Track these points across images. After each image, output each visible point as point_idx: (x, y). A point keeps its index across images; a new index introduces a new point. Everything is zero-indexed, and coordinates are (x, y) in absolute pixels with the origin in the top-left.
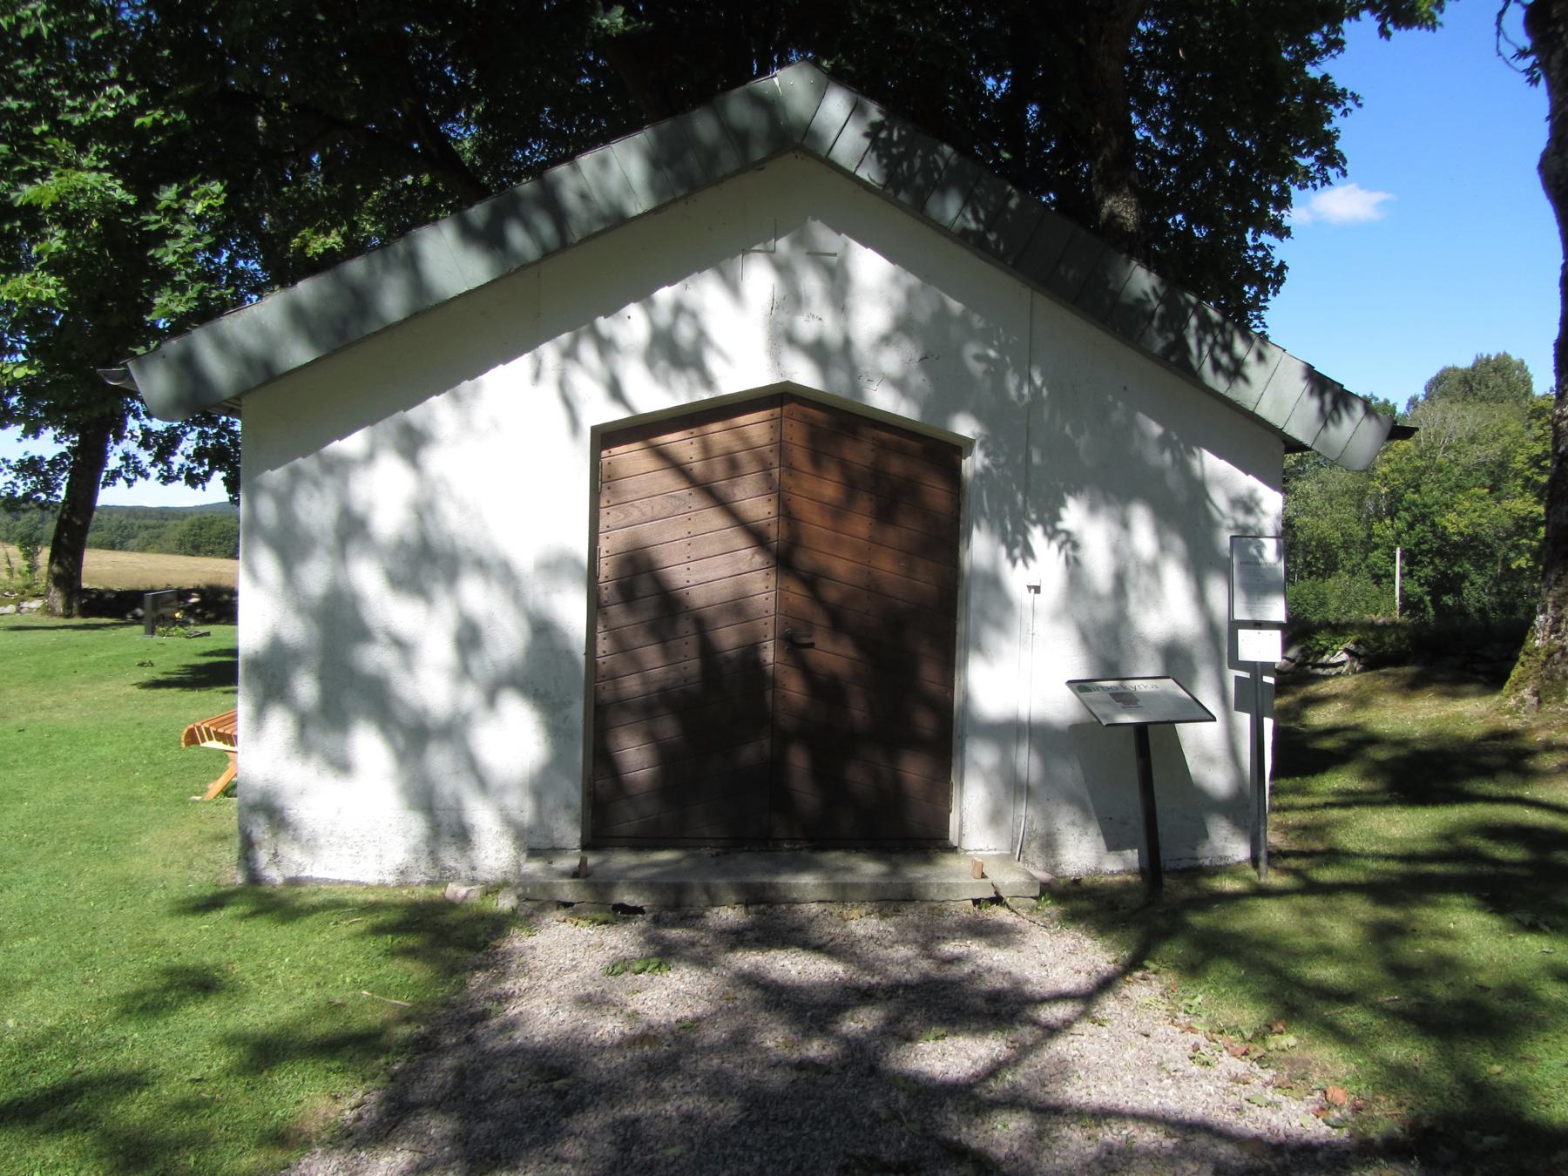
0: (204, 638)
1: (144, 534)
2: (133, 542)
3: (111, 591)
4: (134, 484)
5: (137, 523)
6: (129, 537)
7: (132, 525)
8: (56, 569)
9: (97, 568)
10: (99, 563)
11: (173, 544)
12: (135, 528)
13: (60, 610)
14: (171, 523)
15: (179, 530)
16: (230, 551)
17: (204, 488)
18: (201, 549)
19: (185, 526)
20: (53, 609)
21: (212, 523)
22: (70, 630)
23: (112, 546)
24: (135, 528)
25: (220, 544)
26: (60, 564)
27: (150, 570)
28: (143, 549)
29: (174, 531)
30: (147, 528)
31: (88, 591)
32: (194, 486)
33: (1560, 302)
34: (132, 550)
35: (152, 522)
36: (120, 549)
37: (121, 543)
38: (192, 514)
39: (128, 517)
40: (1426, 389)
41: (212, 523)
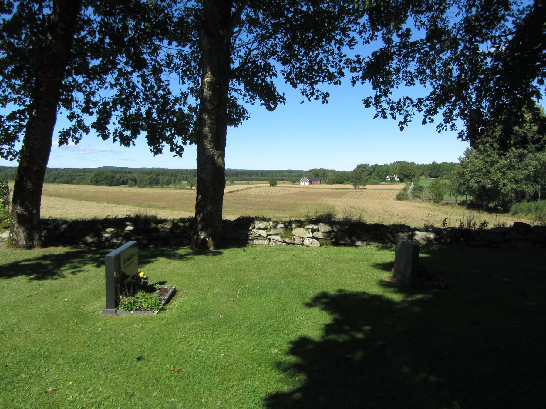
0: (175, 298)
1: (78, 178)
2: (75, 181)
3: (65, 222)
4: (80, 141)
5: (76, 174)
6: (73, 179)
7: (74, 175)
8: (19, 209)
9: (62, 191)
10: (63, 189)
11: (89, 181)
12: (75, 176)
13: (23, 242)
14: (88, 174)
15: (91, 176)
16: (109, 183)
17: (134, 145)
18: (99, 183)
19: (93, 175)
20: (17, 242)
21: (103, 173)
22: (21, 281)
23: (67, 183)
24: (75, 176)
25: (105, 181)
26: (22, 205)
27: (82, 191)
28: (78, 183)
29: (89, 177)
30: (79, 176)
31: (46, 222)
32: (127, 145)
33: (196, 153)
34: (75, 184)
35: (81, 174)
36: (70, 183)
37: (71, 181)
38: (94, 171)
39: (73, 172)
40: (538, 109)
41: (103, 173)
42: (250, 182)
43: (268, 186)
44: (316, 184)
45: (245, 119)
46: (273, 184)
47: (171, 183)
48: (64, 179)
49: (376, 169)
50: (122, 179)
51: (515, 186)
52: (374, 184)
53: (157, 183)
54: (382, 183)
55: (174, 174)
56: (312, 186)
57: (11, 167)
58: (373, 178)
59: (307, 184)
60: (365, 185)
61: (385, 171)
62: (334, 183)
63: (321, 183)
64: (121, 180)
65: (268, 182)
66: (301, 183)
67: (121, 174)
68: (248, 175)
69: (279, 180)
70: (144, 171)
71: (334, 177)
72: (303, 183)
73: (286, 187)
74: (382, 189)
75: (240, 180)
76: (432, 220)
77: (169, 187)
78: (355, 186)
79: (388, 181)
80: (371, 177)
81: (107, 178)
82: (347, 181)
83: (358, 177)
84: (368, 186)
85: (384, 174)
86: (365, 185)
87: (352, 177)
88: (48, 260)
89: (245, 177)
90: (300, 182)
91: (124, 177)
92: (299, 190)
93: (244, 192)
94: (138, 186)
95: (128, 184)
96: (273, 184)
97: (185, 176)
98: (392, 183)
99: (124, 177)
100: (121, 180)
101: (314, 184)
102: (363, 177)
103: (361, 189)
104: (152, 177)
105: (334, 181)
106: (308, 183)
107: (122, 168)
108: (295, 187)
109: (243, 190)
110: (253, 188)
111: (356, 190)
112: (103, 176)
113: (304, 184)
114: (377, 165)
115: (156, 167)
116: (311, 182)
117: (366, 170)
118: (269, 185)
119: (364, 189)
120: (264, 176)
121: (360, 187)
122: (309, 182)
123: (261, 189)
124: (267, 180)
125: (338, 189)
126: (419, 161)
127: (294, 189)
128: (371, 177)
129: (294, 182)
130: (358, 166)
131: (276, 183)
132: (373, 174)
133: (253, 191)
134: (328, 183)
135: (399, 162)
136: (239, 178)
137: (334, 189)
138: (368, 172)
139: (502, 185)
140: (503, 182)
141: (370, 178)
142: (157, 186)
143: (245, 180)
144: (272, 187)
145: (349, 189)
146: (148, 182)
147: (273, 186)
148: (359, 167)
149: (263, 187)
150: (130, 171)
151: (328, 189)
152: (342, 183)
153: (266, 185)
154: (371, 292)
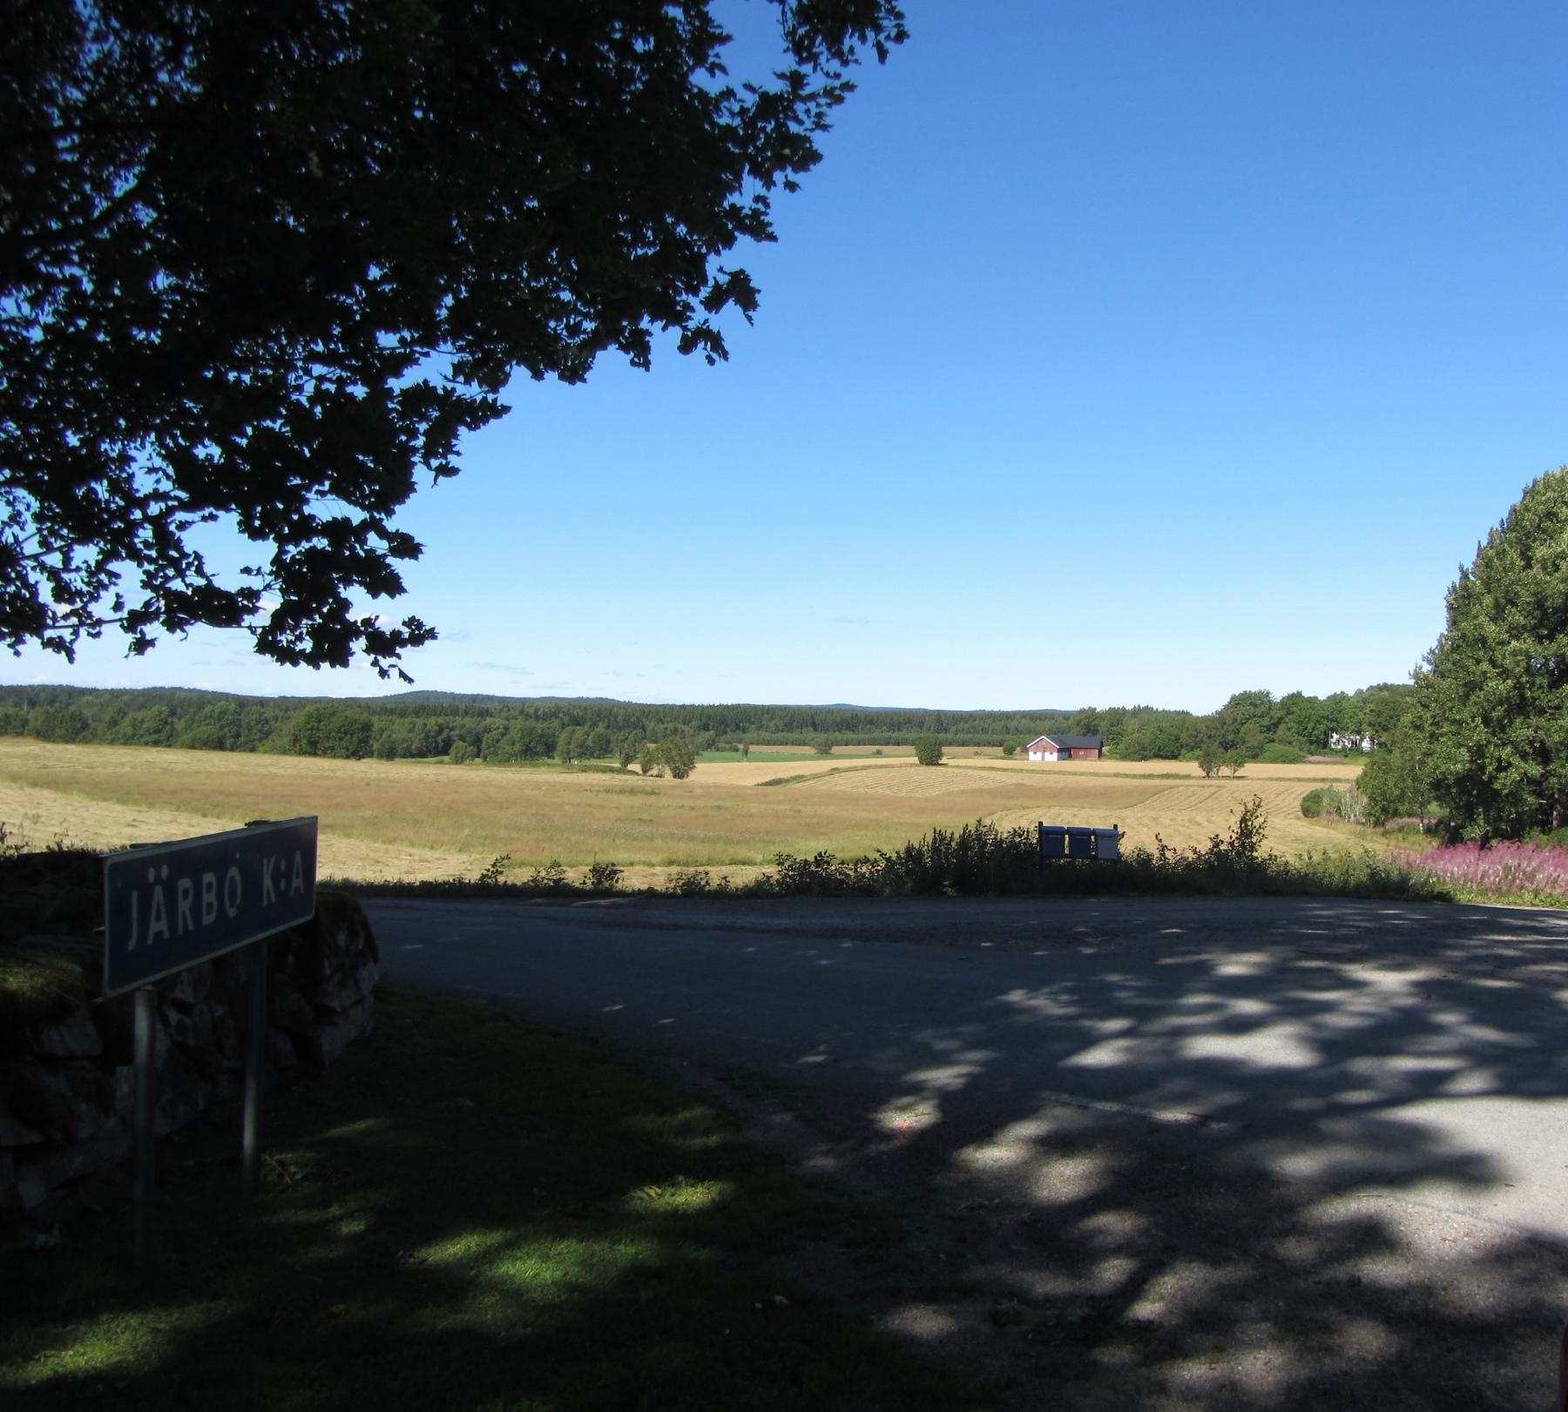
11: (286, 741)
19: (299, 717)
23: (220, 745)
41: (333, 714)
42: (886, 749)
43: (912, 765)
44: (1085, 758)
45: (398, 565)
46: (931, 758)
47: (611, 751)
48: (211, 730)
49: (1294, 709)
50: (445, 734)
51: (1535, 770)
52: (1284, 762)
53: (549, 749)
54: (1312, 758)
55: (633, 719)
56: (1069, 765)
57: (95, 690)
58: (1281, 741)
59: (1052, 757)
60: (1241, 765)
61: (1326, 718)
62: (1145, 758)
63: (1100, 755)
64: (440, 739)
65: (911, 749)
66: (1031, 754)
67: (441, 720)
68: (892, 728)
69: (951, 744)
70: (531, 711)
71: (1146, 739)
72: (1039, 754)
73: (970, 768)
74: (1290, 780)
75: (769, 744)
76: (39, 826)
77: (426, 763)
78: (1208, 764)
79: (1337, 752)
80: (1276, 737)
81: (346, 731)
82: (1192, 749)
83: (1230, 737)
84: (1250, 769)
85: (1322, 728)
86: (1239, 763)
87: (1210, 737)
88: (900, 1133)
89: (876, 734)
90: (1026, 751)
91: (452, 729)
92: (1012, 779)
93: (823, 786)
94: (485, 759)
95: (453, 751)
96: (931, 758)
97: (671, 726)
98: (1347, 760)
99: (452, 729)
100: (440, 739)
101: (1078, 757)
102: (1248, 738)
103: (1338, 780)
104: (533, 729)
105: (1144, 749)
106: (1055, 755)
107: (474, 698)
108: (1005, 770)
109: (816, 776)
110: (855, 769)
111: (1207, 782)
112: (335, 722)
113: (1043, 757)
114: (1299, 695)
115: (592, 695)
116: (1066, 752)
117: (1258, 711)
118: (916, 760)
119: (1238, 778)
120: (946, 730)
121: (1225, 771)
122: (1059, 751)
123: (879, 773)
124: (904, 742)
125: (1150, 776)
126: (1319, 688)
127: (993, 774)
128: (1276, 737)
129: (1009, 752)
130: (1234, 698)
131: (940, 755)
132: (1282, 726)
133: (841, 784)
134: (1126, 756)
135: (1385, 687)
136: (861, 736)
137: (1135, 776)
138: (1266, 721)
139: (1495, 765)
140: (1496, 754)
141: (1272, 741)
142: (551, 761)
143: (873, 742)
144: (925, 768)
145: (1187, 777)
146: (517, 748)
147: (928, 764)
148: (1239, 701)
149: (892, 766)
150: (478, 707)
151: (1116, 775)
152: (1174, 757)
153: (904, 760)
154: (1448, 1195)
